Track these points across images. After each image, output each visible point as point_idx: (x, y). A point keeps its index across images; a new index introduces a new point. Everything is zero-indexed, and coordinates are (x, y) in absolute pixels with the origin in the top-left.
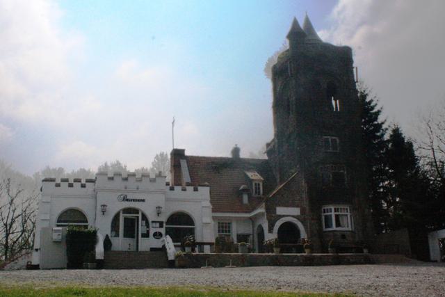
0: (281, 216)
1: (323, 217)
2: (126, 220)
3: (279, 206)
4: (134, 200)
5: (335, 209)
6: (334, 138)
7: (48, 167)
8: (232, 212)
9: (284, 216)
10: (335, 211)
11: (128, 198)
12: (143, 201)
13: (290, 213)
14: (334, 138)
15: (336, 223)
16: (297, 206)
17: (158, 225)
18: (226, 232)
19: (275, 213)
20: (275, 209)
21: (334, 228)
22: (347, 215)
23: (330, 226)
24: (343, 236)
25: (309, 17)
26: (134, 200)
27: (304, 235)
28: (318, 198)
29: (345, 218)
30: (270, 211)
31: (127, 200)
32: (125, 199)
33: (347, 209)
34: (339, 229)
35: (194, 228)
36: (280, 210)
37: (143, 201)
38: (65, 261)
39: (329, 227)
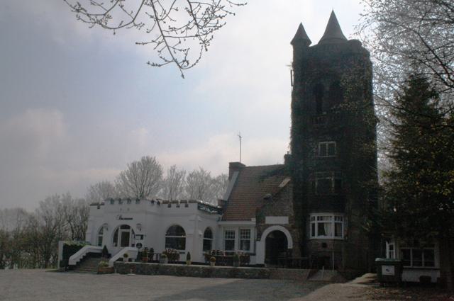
0: (269, 226)
1: (311, 225)
2: (123, 233)
3: (268, 215)
4: (126, 219)
5: (318, 217)
6: (331, 142)
7: (147, 168)
8: (242, 220)
9: (272, 225)
10: (318, 220)
11: (123, 217)
12: (131, 219)
13: (278, 222)
14: (331, 142)
15: (319, 231)
16: (286, 215)
17: (140, 237)
18: (247, 237)
19: (264, 222)
20: (264, 219)
21: (316, 237)
22: (331, 223)
23: (313, 235)
24: (324, 245)
25: (303, 24)
26: (126, 219)
27: (290, 245)
28: (303, 208)
29: (329, 226)
30: (260, 220)
31: (122, 219)
32: (121, 219)
33: (341, 218)
34: (322, 237)
35: (185, 238)
36: (269, 220)
37: (131, 219)
38: (325, 225)
39: (230, 249)
